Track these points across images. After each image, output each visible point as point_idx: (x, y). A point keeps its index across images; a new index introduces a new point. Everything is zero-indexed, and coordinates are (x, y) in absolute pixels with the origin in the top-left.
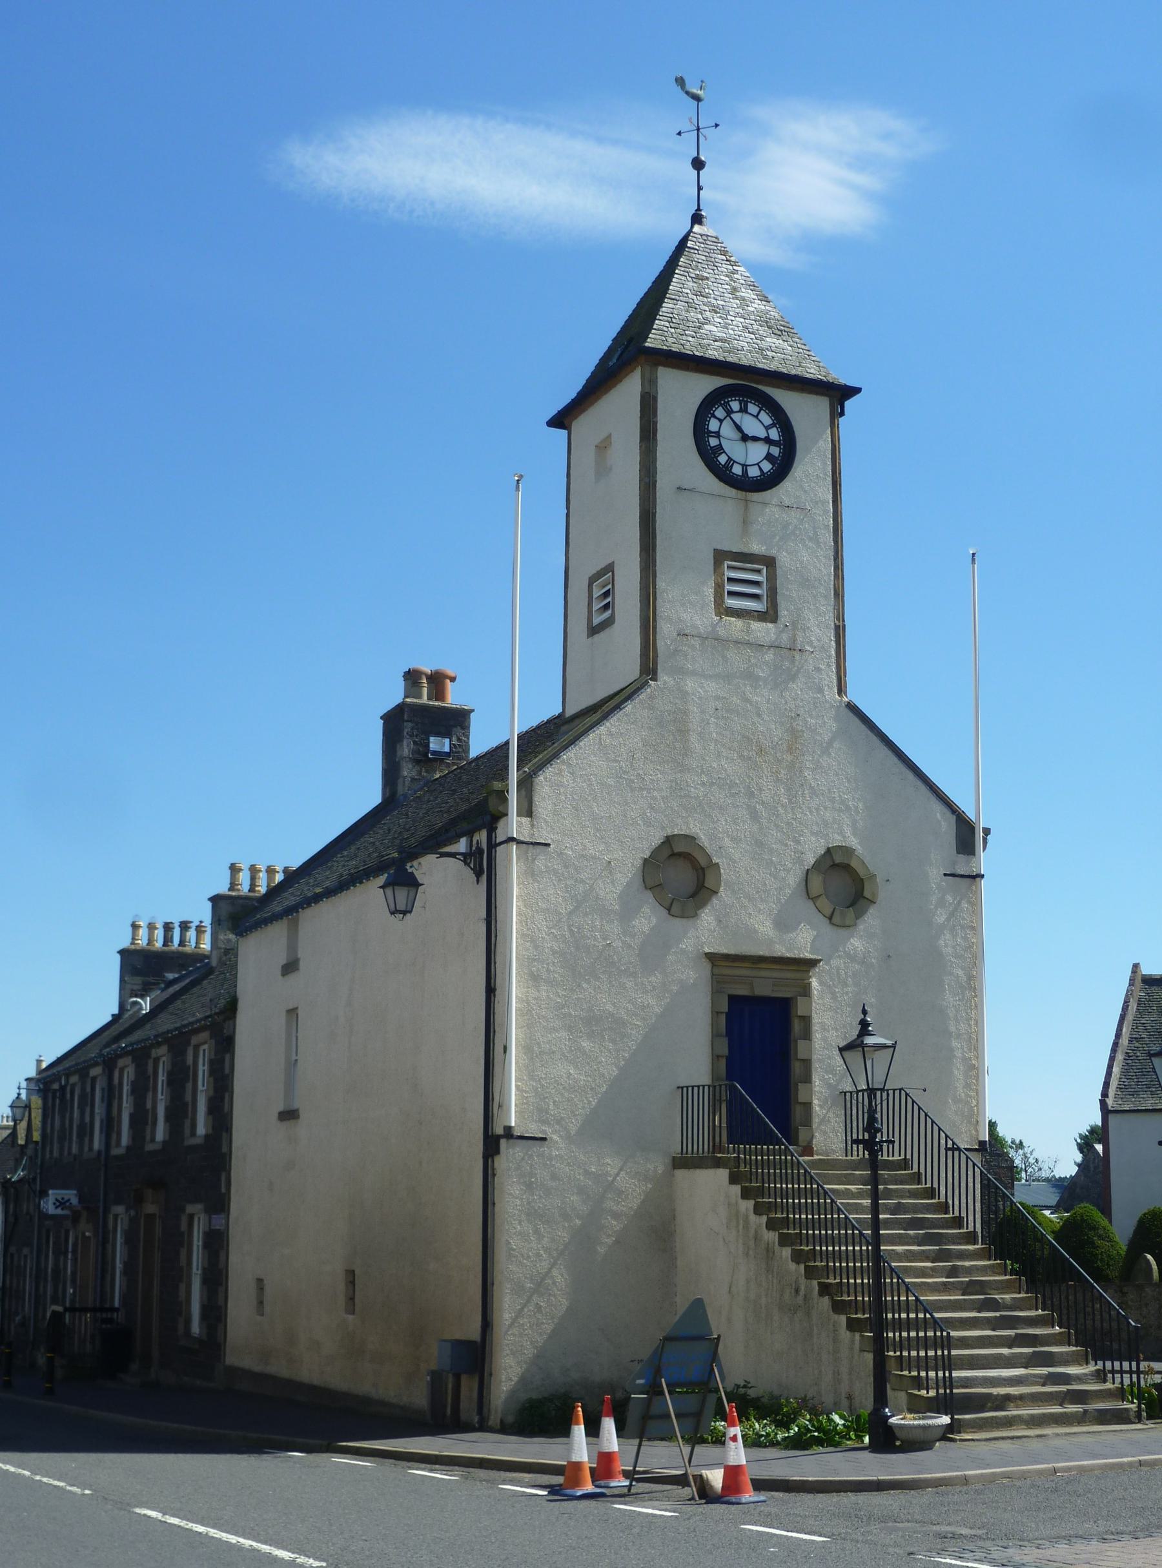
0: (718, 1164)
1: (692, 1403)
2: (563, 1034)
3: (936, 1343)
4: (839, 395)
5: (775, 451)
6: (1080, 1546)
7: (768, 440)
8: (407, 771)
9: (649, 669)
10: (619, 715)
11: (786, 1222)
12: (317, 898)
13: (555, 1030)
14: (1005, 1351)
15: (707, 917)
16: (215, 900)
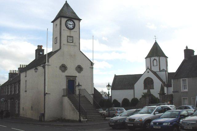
0: (66, 96)
15: (66, 72)
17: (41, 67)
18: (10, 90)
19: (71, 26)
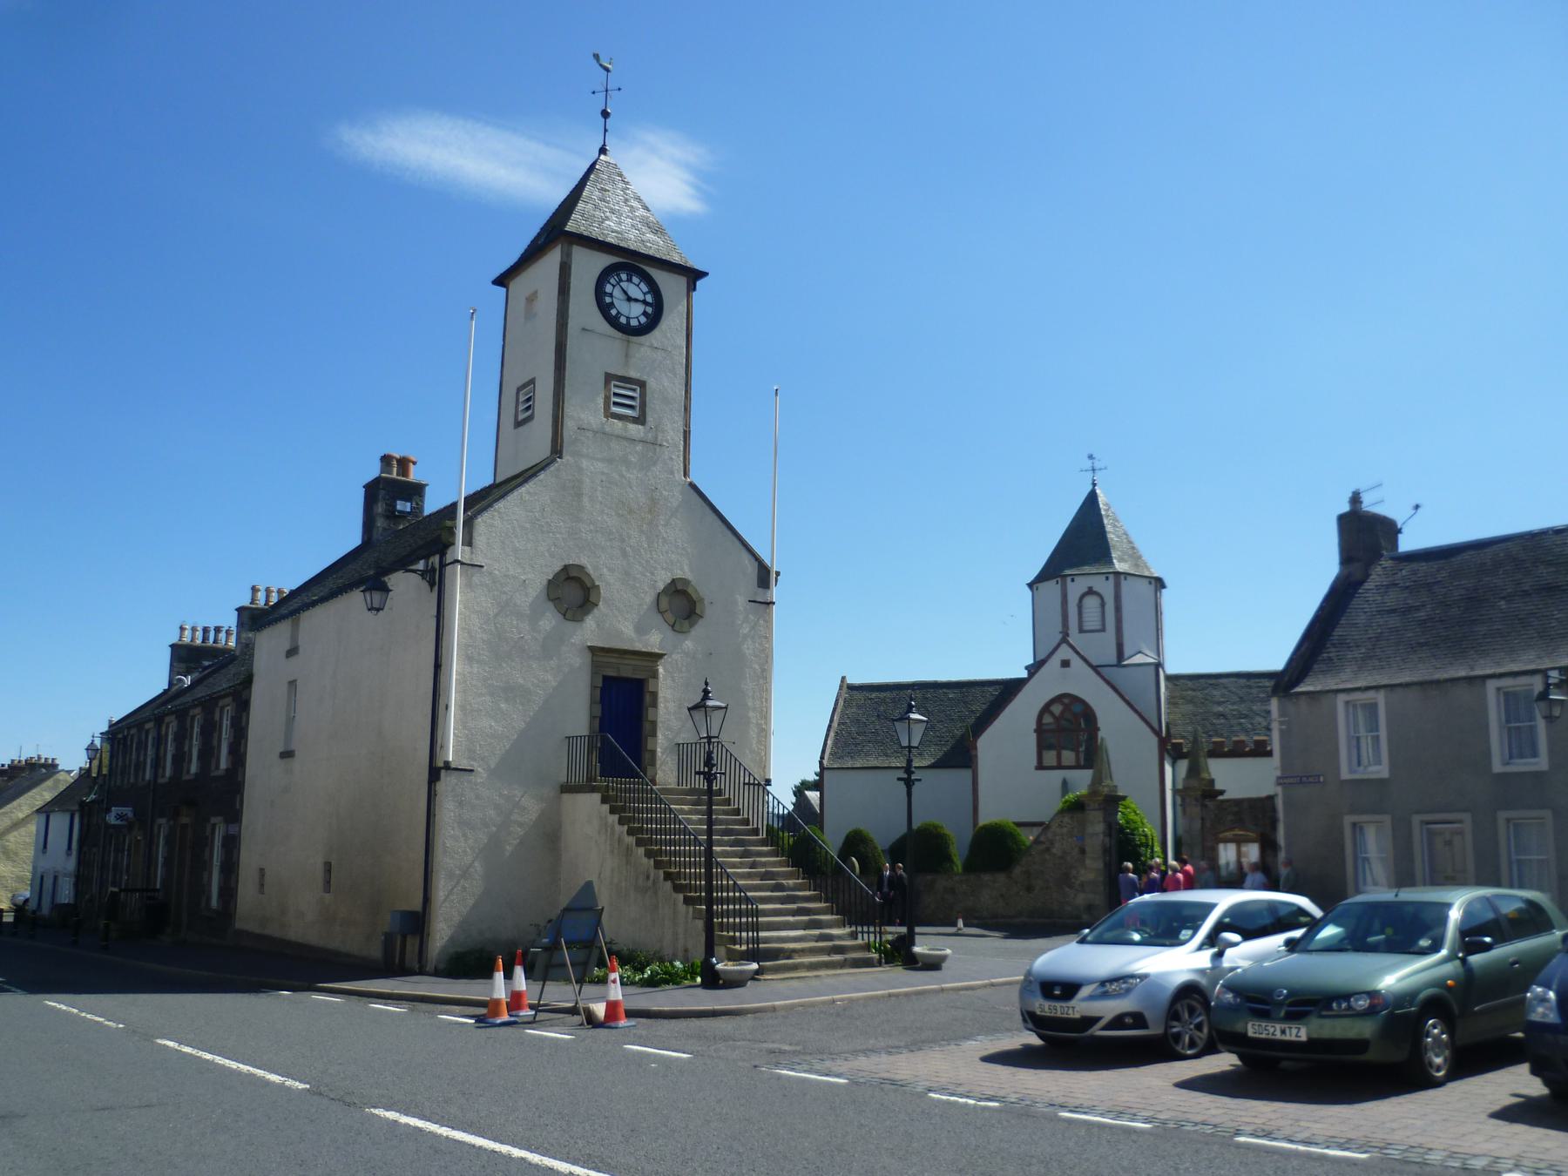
0: (593, 790)
1: (581, 955)
2: (488, 698)
3: (748, 913)
4: (693, 276)
5: (649, 310)
6: (874, 1058)
7: (645, 302)
8: (380, 523)
9: (557, 450)
10: (536, 480)
11: (641, 830)
12: (314, 604)
13: (481, 695)
14: (791, 919)
15: (590, 622)
16: (240, 610)
17: (414, 579)
18: (170, 749)
19: (634, 313)
